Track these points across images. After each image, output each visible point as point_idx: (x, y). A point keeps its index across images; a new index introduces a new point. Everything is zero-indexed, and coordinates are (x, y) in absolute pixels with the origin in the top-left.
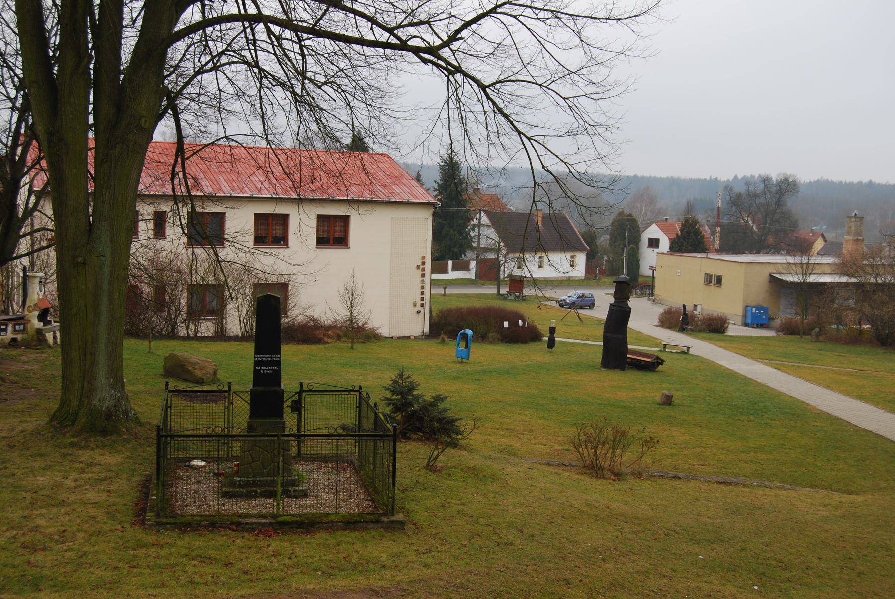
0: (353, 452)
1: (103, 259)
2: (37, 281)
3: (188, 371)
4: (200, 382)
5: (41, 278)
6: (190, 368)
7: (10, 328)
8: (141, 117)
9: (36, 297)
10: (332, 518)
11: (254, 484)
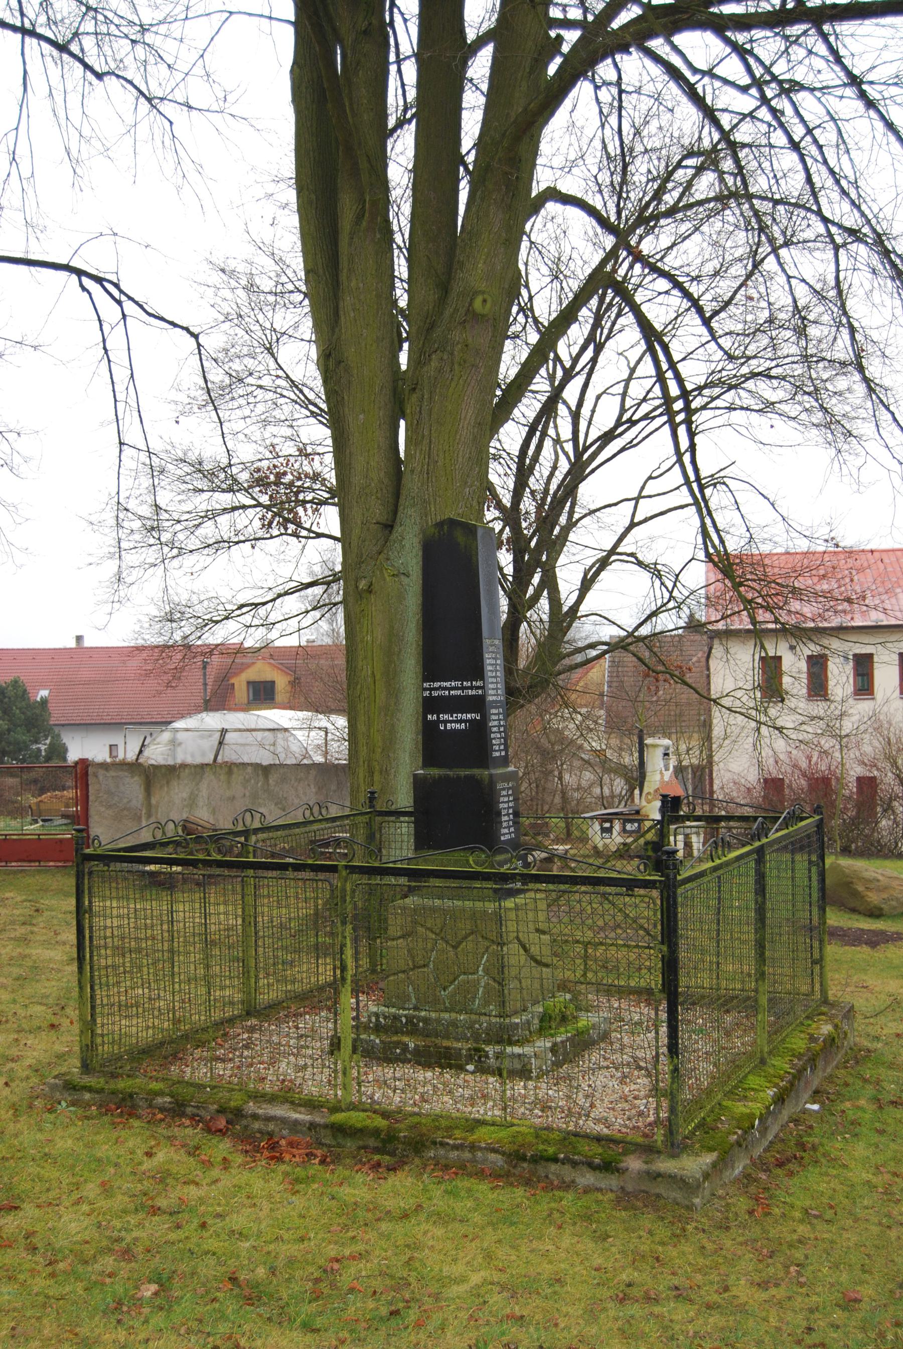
0: (805, 989)
1: (405, 580)
2: (660, 752)
3: (855, 894)
4: (875, 913)
5: (667, 748)
6: (860, 888)
7: (617, 826)
8: (476, 293)
9: (658, 777)
10: (483, 1135)
11: (411, 1027)
